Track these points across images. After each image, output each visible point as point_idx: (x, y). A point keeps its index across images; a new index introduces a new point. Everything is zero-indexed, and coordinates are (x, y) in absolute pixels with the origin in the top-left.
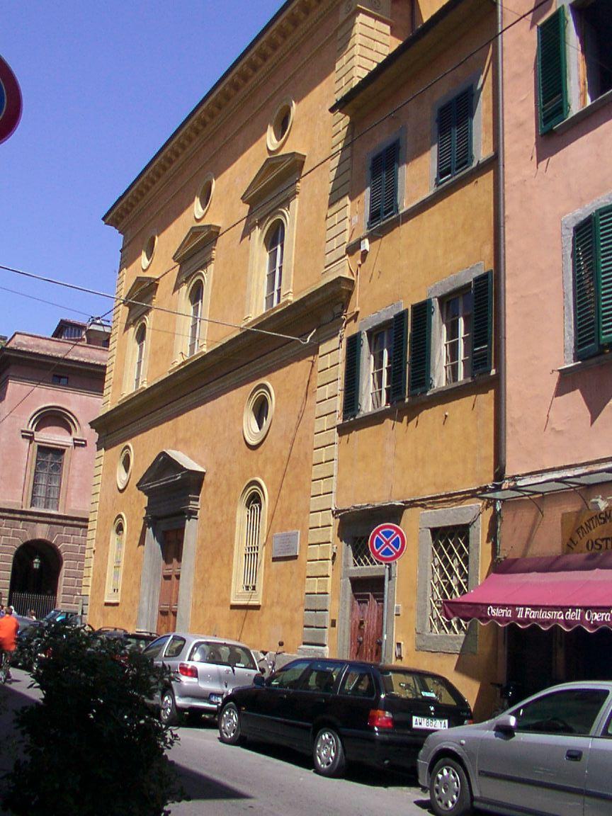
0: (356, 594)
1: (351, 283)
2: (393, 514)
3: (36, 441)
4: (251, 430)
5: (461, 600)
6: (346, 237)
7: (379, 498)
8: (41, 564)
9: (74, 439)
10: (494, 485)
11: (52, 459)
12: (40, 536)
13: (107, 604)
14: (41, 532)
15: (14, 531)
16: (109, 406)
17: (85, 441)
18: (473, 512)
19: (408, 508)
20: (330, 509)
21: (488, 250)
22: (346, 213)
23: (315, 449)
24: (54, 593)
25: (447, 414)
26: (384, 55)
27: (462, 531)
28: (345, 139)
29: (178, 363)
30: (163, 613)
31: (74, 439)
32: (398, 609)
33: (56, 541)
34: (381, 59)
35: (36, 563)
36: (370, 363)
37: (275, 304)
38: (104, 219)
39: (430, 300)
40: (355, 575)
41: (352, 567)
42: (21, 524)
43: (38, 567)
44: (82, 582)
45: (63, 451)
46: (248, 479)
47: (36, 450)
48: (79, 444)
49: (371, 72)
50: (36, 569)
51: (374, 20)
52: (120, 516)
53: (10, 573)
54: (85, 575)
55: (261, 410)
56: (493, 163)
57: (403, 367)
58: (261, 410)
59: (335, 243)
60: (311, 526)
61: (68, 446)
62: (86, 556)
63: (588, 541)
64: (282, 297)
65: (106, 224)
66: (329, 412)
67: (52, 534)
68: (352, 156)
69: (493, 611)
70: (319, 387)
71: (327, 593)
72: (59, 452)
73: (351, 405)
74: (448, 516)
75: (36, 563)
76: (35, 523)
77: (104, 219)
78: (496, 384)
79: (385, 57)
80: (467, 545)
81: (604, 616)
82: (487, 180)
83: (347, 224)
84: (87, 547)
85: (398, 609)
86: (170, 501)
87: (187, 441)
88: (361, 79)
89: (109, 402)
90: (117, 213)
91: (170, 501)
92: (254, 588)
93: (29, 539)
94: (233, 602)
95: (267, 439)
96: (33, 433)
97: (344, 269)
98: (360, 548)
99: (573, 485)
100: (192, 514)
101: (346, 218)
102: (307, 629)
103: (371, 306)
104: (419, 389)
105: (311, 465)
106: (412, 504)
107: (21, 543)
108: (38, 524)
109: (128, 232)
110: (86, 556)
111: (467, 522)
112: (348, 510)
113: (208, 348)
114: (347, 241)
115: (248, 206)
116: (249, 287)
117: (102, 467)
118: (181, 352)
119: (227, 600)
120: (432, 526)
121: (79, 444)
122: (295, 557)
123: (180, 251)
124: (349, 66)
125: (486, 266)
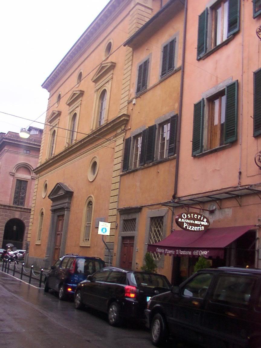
2: (139, 210)
4: (91, 178)
5: (155, 244)
6: (127, 98)
7: (134, 204)
8: (16, 228)
13: (36, 245)
14: (17, 215)
15: (6, 214)
21: (177, 105)
23: (112, 184)
24: (22, 241)
25: (159, 171)
27: (161, 218)
31: (32, 177)
32: (137, 250)
34: (148, 20)
35: (15, 228)
38: (42, 86)
40: (123, 236)
42: (8, 211)
47: (16, 181)
52: (42, 209)
53: (3, 232)
54: (29, 233)
56: (182, 68)
62: (30, 225)
67: (21, 215)
68: (132, 65)
69: (158, 250)
70: (115, 159)
73: (195, 144)
74: (156, 213)
75: (15, 228)
76: (15, 211)
77: (42, 86)
78: (178, 159)
79: (142, 26)
81: (199, 252)
82: (178, 76)
85: (137, 250)
88: (146, 22)
93: (12, 218)
94: (81, 245)
96: (14, 174)
99: (214, 199)
103: (139, 124)
105: (110, 190)
106: (144, 206)
107: (9, 219)
108: (16, 212)
109: (51, 92)
110: (30, 225)
111: (163, 215)
123: (94, 77)
125: (176, 112)
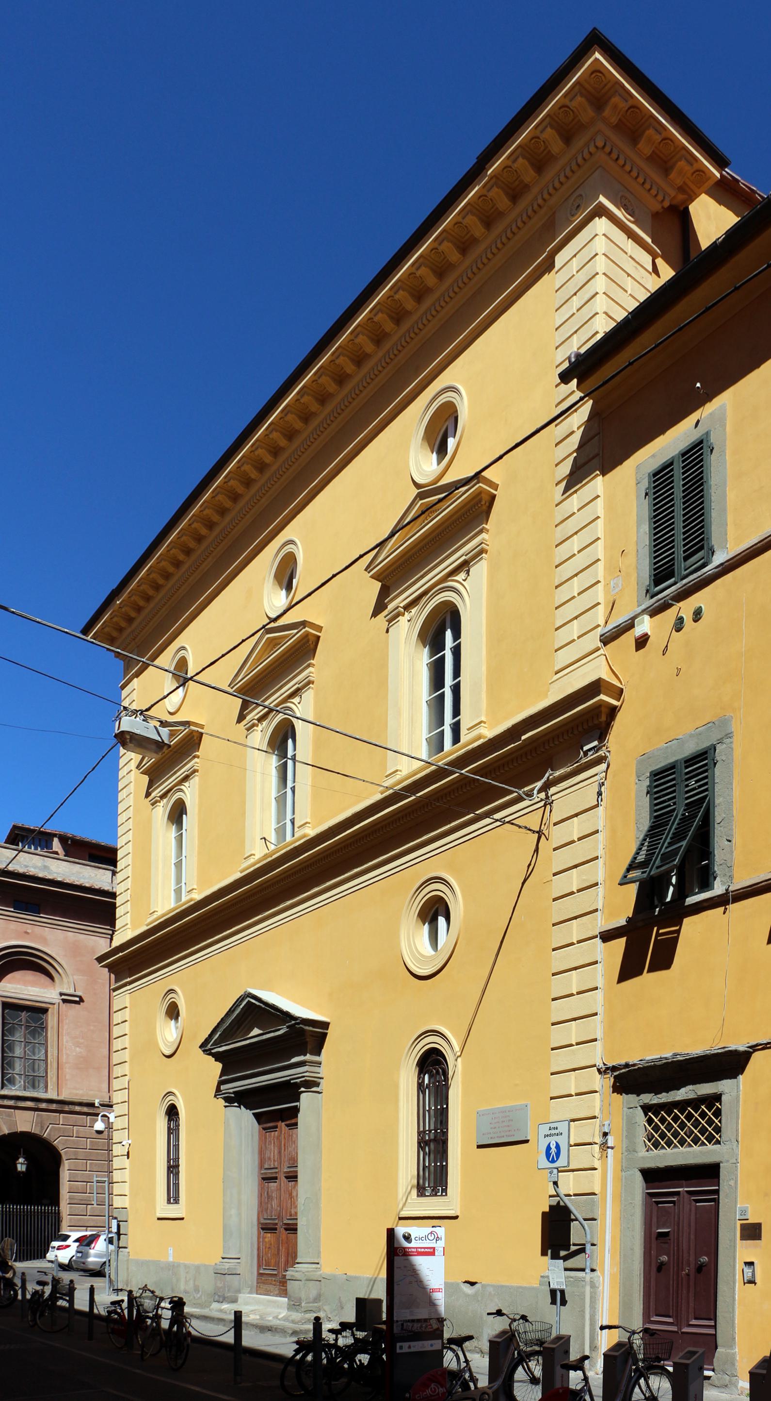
4: (417, 945)
11: (27, 1022)
16: (601, 304)
17: (80, 997)
19: (755, 1051)
20: (595, 1066)
22: (597, 574)
24: (56, 1201)
28: (577, 451)
29: (257, 857)
30: (267, 1228)
33: (49, 1134)
37: (289, 838)
38: (169, 1202)
41: (642, 1152)
43: (24, 1169)
45: (45, 1011)
48: (72, 1000)
50: (23, 1172)
51: (626, 237)
55: (434, 911)
58: (434, 911)
59: (575, 629)
64: (296, 829)
71: (594, 1194)
72: (38, 1012)
83: (599, 594)
86: (266, 1061)
87: (279, 965)
89: (129, 926)
91: (266, 1061)
97: (596, 669)
98: (663, 1122)
100: (311, 1084)
101: (598, 582)
112: (634, 1065)
113: (134, 928)
114: (601, 622)
115: (378, 585)
116: (382, 721)
117: (128, 914)
118: (261, 839)
121: (72, 1000)
122: (527, 1141)
124: (586, 313)
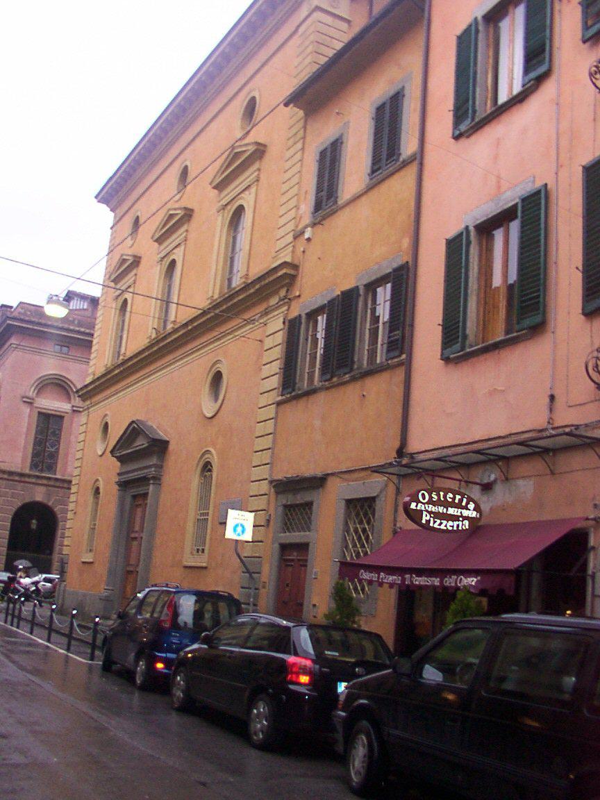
0: (596, 718)
1: (295, 267)
2: (318, 482)
3: (36, 407)
7: (308, 469)
8: (38, 525)
9: (73, 406)
10: (396, 461)
12: (39, 498)
13: (83, 563)
14: (39, 495)
15: (13, 493)
18: (373, 485)
21: (406, 243)
25: (365, 393)
26: (318, 64)
27: (370, 501)
31: (73, 406)
32: (316, 573)
36: (307, 344)
38: (96, 197)
39: (357, 287)
42: (20, 486)
44: (63, 541)
45: (62, 418)
46: (203, 448)
49: (322, 65)
52: (97, 480)
53: (8, 532)
56: (419, 158)
57: (350, 345)
60: (252, 494)
61: (67, 413)
63: (24, 402)
65: (99, 202)
66: (271, 389)
70: (264, 365)
74: (358, 489)
77: (96, 197)
78: (408, 366)
79: (327, 59)
80: (373, 517)
82: (410, 174)
84: (70, 509)
85: (316, 573)
88: (335, 52)
90: (134, 160)
92: (203, 550)
94: (186, 564)
95: (222, 408)
96: (33, 399)
102: (244, 590)
103: (319, 284)
104: (342, 370)
106: (333, 474)
108: (37, 487)
109: (118, 211)
111: (375, 495)
119: (181, 561)
120: (346, 498)
125: (405, 258)
